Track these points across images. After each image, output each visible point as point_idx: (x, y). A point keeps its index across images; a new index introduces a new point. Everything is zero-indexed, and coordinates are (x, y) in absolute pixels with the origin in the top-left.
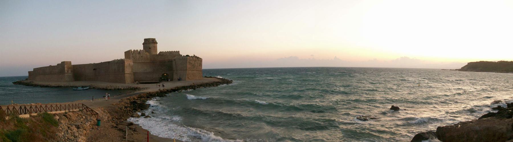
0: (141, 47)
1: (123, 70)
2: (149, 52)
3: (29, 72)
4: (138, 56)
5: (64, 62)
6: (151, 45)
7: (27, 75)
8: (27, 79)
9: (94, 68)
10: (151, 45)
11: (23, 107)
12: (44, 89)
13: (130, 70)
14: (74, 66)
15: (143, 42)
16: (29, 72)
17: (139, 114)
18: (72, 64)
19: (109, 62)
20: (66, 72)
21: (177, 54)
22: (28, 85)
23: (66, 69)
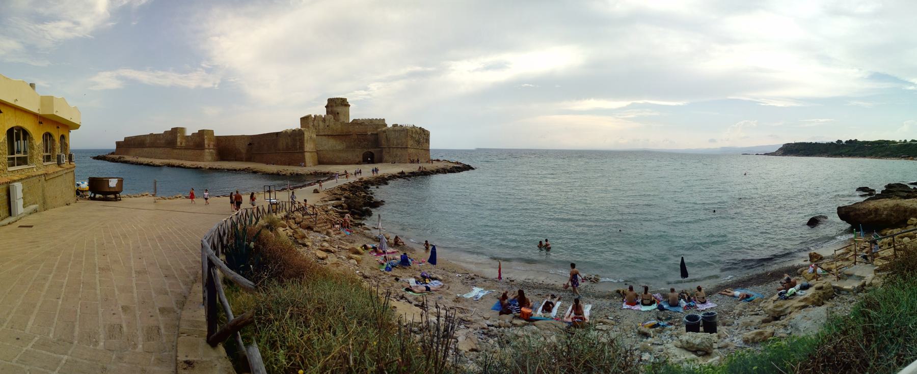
0: (323, 112)
1: (302, 146)
2: (336, 120)
3: (118, 144)
4: (321, 124)
5: (176, 129)
6: (339, 109)
7: (113, 147)
8: (113, 153)
9: (810, 213)
10: (339, 109)
11: (65, 160)
12: (147, 169)
13: (312, 146)
14: (218, 138)
15: (326, 103)
16: (118, 144)
17: (784, 343)
18: (215, 135)
19: (277, 134)
20: (206, 146)
21: (382, 123)
22: (113, 160)
23: (206, 142)
